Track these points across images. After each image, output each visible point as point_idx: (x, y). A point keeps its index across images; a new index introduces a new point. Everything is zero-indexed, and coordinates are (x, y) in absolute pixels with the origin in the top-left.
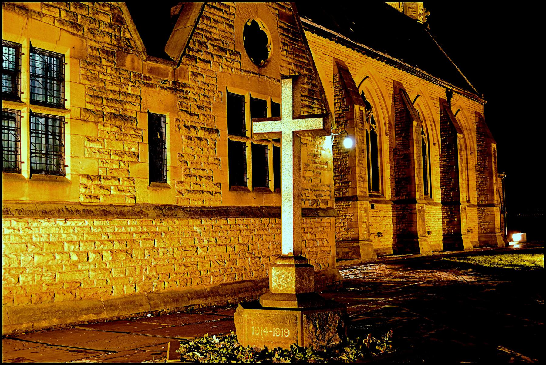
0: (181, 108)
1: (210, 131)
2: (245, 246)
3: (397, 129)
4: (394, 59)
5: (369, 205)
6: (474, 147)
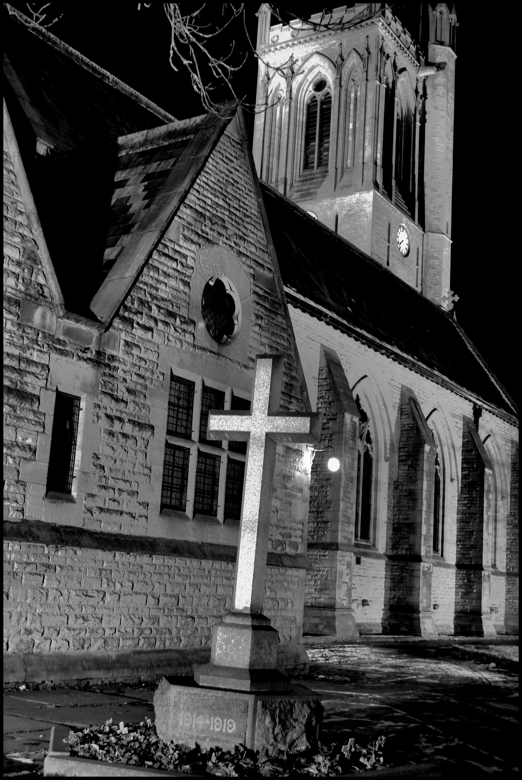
0: (104, 390)
1: (141, 426)
2: (174, 599)
3: (401, 454)
4: (405, 355)
5: (354, 559)
6: (506, 489)
